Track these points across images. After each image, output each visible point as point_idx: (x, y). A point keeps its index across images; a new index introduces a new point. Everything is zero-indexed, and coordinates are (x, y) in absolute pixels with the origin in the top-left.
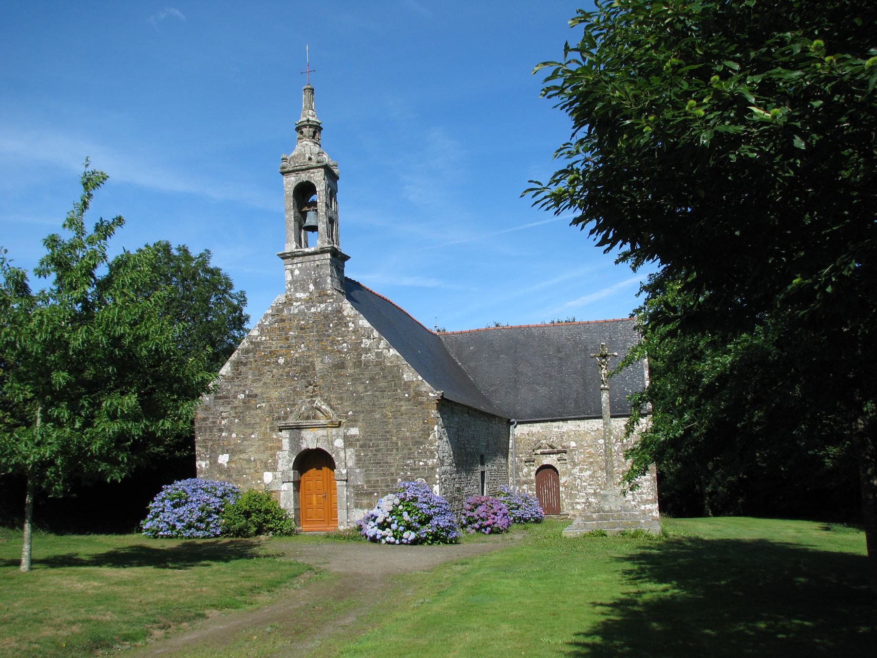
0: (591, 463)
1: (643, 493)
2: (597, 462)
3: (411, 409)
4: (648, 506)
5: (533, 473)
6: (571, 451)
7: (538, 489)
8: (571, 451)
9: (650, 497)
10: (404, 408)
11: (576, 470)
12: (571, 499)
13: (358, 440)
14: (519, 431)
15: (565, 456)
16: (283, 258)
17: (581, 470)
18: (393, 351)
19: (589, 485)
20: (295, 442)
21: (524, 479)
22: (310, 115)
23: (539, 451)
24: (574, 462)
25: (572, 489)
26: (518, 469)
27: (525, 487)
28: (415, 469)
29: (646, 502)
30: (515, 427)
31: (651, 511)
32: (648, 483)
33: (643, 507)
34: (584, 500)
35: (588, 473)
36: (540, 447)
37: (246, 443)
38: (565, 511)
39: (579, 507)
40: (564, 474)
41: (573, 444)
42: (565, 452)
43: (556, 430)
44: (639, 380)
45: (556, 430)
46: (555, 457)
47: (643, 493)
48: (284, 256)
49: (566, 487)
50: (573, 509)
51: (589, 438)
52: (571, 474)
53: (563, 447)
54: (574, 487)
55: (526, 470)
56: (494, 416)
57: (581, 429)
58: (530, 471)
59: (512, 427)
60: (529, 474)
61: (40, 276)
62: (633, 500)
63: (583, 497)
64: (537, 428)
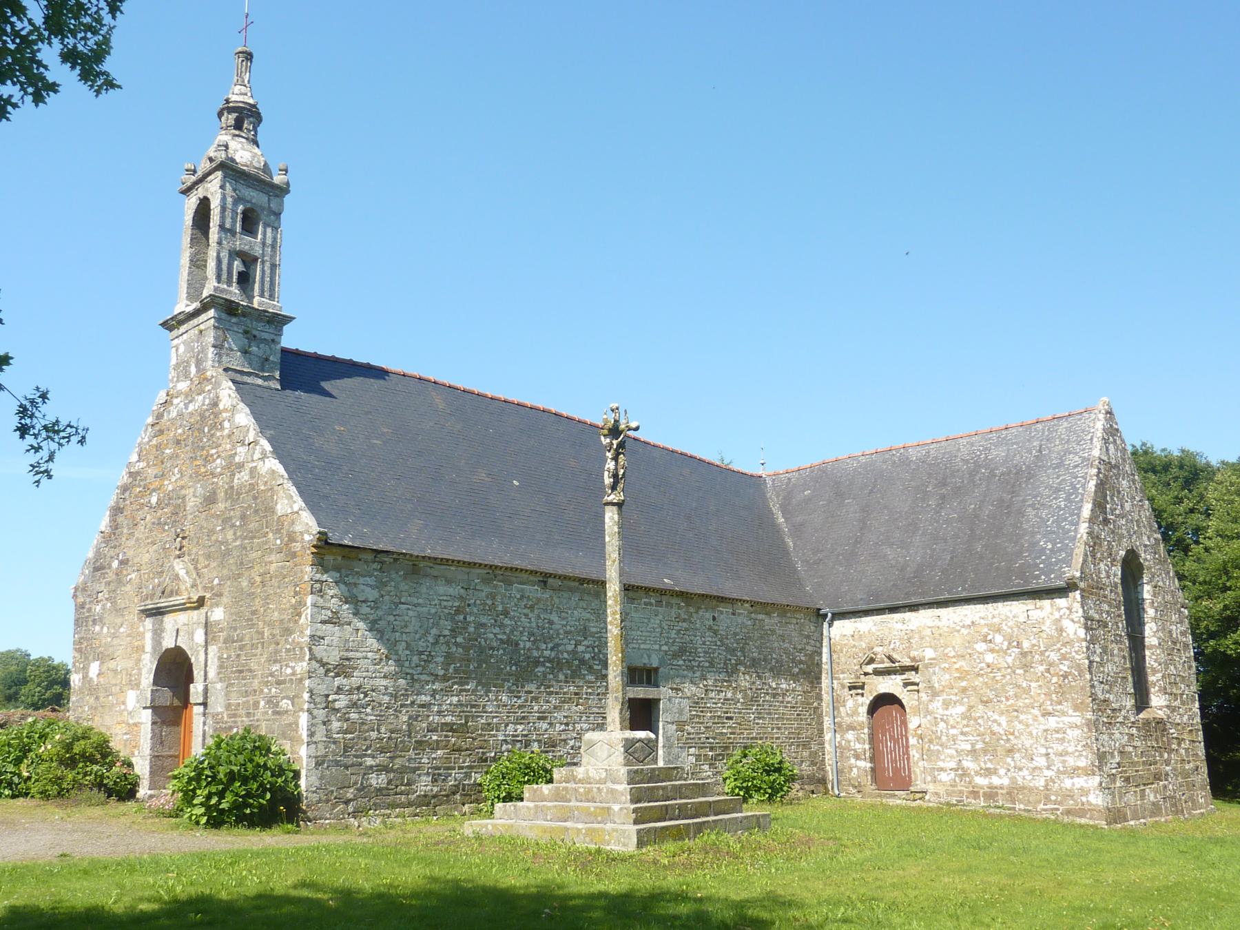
0: (964, 690)
1: (1067, 753)
2: (974, 688)
3: (282, 567)
4: (1080, 782)
5: (863, 710)
6: (926, 666)
7: (873, 739)
8: (926, 666)
9: (1082, 763)
10: (273, 567)
11: (937, 705)
12: (929, 760)
13: (221, 630)
14: (840, 630)
15: (912, 676)
16: (171, 329)
17: (946, 704)
18: (274, 464)
19: (962, 733)
20: (158, 634)
21: (848, 720)
22: (238, 95)
23: (869, 669)
24: (931, 687)
25: (931, 741)
26: (836, 703)
27: (850, 735)
28: (283, 682)
29: (1074, 772)
30: (830, 625)
31: (1084, 792)
32: (1077, 732)
33: (1068, 783)
34: (953, 765)
35: (961, 709)
36: (871, 661)
37: (115, 642)
38: (919, 785)
39: (944, 777)
40: (917, 711)
41: (929, 654)
42: (916, 669)
43: (899, 626)
44: (1072, 524)
45: (899, 626)
46: (898, 679)
47: (1067, 753)
48: (169, 325)
49: (921, 737)
50: (935, 781)
51: (957, 641)
52: (928, 712)
53: (913, 659)
54: (935, 738)
55: (850, 703)
56: (722, 600)
57: (943, 623)
58: (857, 706)
59: (826, 625)
60: (855, 713)
61: (20, 412)
62: (1048, 768)
63: (952, 757)
64: (866, 624)
